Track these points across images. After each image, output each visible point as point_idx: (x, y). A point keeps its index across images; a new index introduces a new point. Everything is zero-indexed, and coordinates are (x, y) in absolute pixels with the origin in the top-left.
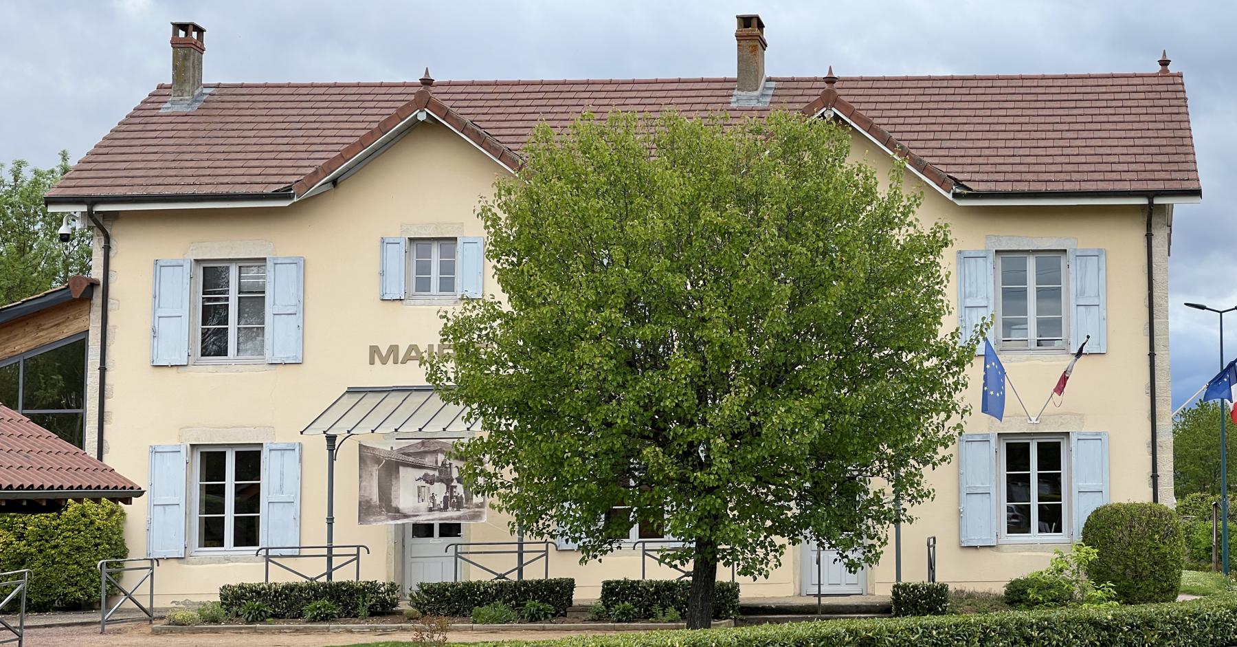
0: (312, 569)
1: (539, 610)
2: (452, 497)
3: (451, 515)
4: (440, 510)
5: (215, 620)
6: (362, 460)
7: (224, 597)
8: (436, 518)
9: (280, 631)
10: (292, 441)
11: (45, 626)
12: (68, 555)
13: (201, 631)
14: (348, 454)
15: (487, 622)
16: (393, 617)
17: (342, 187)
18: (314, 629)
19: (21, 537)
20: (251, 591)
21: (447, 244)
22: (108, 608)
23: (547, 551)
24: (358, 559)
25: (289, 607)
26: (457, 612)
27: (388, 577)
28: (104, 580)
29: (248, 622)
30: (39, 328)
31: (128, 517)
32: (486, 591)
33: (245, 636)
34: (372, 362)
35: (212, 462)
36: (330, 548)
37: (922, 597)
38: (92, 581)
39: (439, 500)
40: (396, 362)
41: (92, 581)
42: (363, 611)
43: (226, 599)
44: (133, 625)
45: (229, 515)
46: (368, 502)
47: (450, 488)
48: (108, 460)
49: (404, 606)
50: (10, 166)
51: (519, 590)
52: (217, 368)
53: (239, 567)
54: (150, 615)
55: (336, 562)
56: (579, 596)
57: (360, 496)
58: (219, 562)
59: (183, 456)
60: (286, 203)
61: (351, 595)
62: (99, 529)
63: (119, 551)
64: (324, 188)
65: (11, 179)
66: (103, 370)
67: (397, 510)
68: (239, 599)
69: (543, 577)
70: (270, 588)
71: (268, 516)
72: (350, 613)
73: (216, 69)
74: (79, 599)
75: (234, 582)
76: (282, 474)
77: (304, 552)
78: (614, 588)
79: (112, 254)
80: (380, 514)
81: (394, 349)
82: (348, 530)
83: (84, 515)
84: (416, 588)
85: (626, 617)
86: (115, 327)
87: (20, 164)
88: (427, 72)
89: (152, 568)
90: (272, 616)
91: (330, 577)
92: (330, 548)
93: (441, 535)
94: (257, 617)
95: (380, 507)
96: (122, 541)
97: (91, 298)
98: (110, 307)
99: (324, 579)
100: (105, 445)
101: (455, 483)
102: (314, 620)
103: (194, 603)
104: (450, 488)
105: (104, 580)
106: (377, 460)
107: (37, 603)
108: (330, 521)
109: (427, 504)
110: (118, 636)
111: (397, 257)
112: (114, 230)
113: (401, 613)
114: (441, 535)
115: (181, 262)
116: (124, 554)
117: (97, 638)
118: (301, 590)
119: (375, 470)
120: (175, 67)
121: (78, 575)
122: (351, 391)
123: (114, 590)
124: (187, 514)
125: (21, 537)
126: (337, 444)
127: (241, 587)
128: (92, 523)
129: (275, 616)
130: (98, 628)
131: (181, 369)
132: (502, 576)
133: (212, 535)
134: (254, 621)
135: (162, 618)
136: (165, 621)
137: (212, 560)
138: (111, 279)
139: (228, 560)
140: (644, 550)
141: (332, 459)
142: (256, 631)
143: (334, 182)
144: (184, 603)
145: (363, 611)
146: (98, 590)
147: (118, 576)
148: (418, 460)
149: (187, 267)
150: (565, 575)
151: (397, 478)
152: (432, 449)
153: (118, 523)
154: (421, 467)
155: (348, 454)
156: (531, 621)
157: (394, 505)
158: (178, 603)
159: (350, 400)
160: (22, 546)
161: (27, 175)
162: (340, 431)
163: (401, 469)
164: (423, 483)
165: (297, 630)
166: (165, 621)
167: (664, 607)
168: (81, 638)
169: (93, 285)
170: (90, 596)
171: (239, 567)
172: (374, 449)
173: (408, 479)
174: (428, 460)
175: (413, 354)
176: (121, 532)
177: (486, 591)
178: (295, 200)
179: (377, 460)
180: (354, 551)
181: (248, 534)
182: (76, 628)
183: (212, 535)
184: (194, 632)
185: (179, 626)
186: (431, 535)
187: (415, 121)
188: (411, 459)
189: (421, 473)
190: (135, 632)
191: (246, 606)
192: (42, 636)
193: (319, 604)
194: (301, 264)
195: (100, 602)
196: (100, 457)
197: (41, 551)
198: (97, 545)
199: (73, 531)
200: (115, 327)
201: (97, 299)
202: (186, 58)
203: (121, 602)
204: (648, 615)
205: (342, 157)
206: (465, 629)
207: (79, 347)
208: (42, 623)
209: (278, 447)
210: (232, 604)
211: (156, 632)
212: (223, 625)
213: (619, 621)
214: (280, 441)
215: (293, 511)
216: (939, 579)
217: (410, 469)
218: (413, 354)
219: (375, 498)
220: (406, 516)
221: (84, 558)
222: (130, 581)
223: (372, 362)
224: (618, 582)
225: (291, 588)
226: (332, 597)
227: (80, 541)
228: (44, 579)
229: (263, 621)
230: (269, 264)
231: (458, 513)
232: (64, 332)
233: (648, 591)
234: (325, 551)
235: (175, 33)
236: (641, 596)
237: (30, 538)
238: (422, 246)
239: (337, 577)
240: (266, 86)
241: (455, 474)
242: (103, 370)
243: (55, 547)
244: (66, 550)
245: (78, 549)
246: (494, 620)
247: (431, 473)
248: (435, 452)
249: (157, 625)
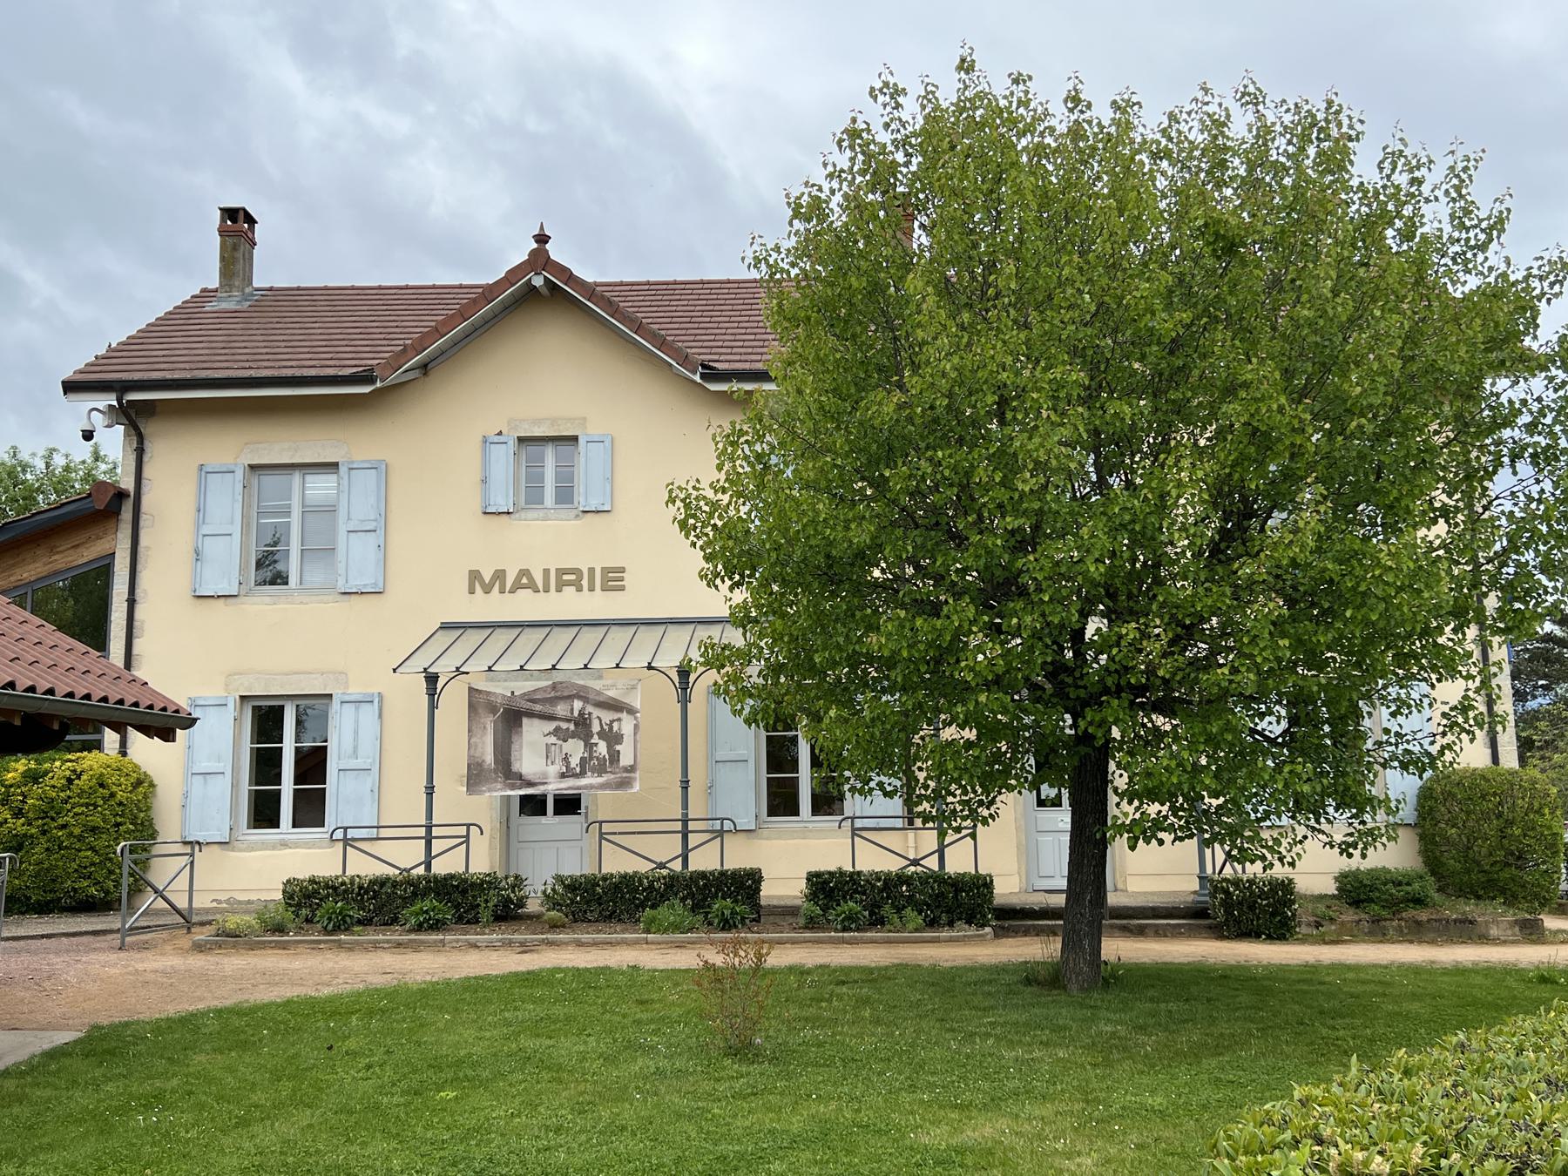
0: (404, 857)
2: (591, 758)
4: (576, 776)
5: (279, 929)
6: (472, 708)
7: (288, 896)
8: (554, 787)
9: (376, 946)
10: (370, 691)
11: (43, 937)
12: (80, 838)
13: (263, 945)
14: (454, 700)
15: (665, 931)
17: (435, 375)
18: (422, 942)
19: (18, 813)
20: (327, 887)
21: (565, 449)
22: (132, 909)
24: (467, 842)
25: (379, 910)
26: (610, 917)
27: (492, 867)
28: (126, 870)
29: (325, 931)
30: (52, 551)
31: (159, 790)
32: (651, 886)
33: (329, 955)
34: (472, 591)
35: (267, 720)
36: (429, 828)
37: (1263, 895)
38: (111, 872)
39: (575, 761)
40: (502, 592)
41: (111, 872)
42: (485, 916)
43: (291, 897)
44: (165, 935)
46: (480, 765)
47: (590, 747)
48: (140, 673)
49: (533, 906)
50: (42, 452)
54: (187, 920)
55: (437, 845)
56: (770, 892)
58: (274, 848)
59: (231, 711)
60: (366, 389)
61: (464, 892)
62: (121, 804)
63: (145, 830)
64: (411, 375)
65: (43, 466)
66: (132, 602)
67: (520, 777)
68: (309, 897)
69: (462, 870)
70: (352, 883)
71: (335, 784)
73: (268, 271)
74: (93, 896)
75: (303, 874)
76: (356, 732)
77: (384, 833)
78: (826, 882)
79: (146, 458)
81: (500, 575)
82: (454, 803)
83: (102, 785)
84: (550, 881)
85: (850, 923)
86: (148, 548)
87: (52, 451)
88: (542, 228)
89: (192, 855)
90: (360, 922)
92: (429, 828)
93: (556, 813)
94: (341, 924)
95: (495, 771)
96: (151, 820)
97: (118, 513)
98: (142, 523)
99: (421, 870)
100: (136, 624)
101: (595, 739)
102: (419, 928)
103: (240, 902)
104: (590, 747)
105: (126, 870)
106: (493, 709)
107: (38, 901)
108: (430, 791)
109: (558, 767)
110: (148, 954)
111: (503, 458)
112: (148, 428)
114: (556, 813)
115: (232, 468)
116: (153, 835)
117: (113, 957)
118: (395, 884)
119: (489, 723)
120: (222, 259)
121: (93, 864)
122: (445, 627)
123: (139, 885)
125: (18, 813)
126: (439, 686)
127: (312, 881)
128: (113, 795)
130: (115, 939)
131: (230, 600)
132: (662, 866)
133: (264, 813)
134: (337, 929)
135: (202, 924)
137: (264, 846)
138: (145, 489)
139: (285, 845)
140: (601, 834)
141: (433, 707)
142: (340, 945)
143: (424, 368)
144: (227, 901)
145: (485, 916)
146: (118, 884)
147: (144, 864)
148: (548, 709)
149: (239, 474)
150: (747, 864)
153: (146, 797)
155: (454, 700)
156: (723, 929)
157: (515, 767)
158: (219, 902)
159: (447, 637)
160: (19, 825)
161: (59, 461)
162: (444, 668)
163: (525, 721)
164: (553, 739)
165: (399, 945)
166: (211, 929)
167: (899, 910)
168: (93, 956)
169: (121, 495)
170: (107, 892)
172: (489, 693)
173: (534, 733)
174: (561, 709)
175: (524, 580)
176: (149, 808)
177: (651, 886)
178: (379, 384)
180: (462, 831)
181: (311, 810)
182: (85, 939)
183: (264, 813)
184: (253, 947)
187: (531, 289)
188: (538, 707)
189: (552, 726)
190: (168, 948)
191: (321, 909)
192: (36, 953)
193: (426, 905)
194: (381, 469)
195: (120, 900)
196: (128, 664)
197: (44, 833)
198: (118, 825)
199: (87, 805)
200: (148, 548)
201: (127, 514)
202: (235, 248)
203: (148, 900)
204: (878, 922)
205: (437, 332)
206: (636, 942)
207: (104, 570)
208: (40, 932)
210: (299, 906)
211: (199, 948)
212: (291, 937)
213: (844, 930)
214: (355, 691)
215: (369, 781)
216: (858, 868)
217: (536, 721)
218: (524, 580)
220: (531, 784)
221: (100, 843)
222: (165, 870)
223: (472, 591)
224: (830, 873)
225: (382, 882)
226: (438, 894)
227: (96, 820)
228: (48, 870)
229: (347, 930)
230: (343, 469)
231: (600, 780)
232: (88, 554)
233: (874, 886)
235: (223, 220)
236: (864, 893)
237: (31, 815)
238: (533, 449)
239: (440, 867)
240: (326, 288)
241: (596, 728)
242: (132, 602)
243: (64, 827)
244: (77, 831)
245: (94, 830)
246: (676, 927)
247: (564, 725)
248: (571, 698)
249: (201, 935)
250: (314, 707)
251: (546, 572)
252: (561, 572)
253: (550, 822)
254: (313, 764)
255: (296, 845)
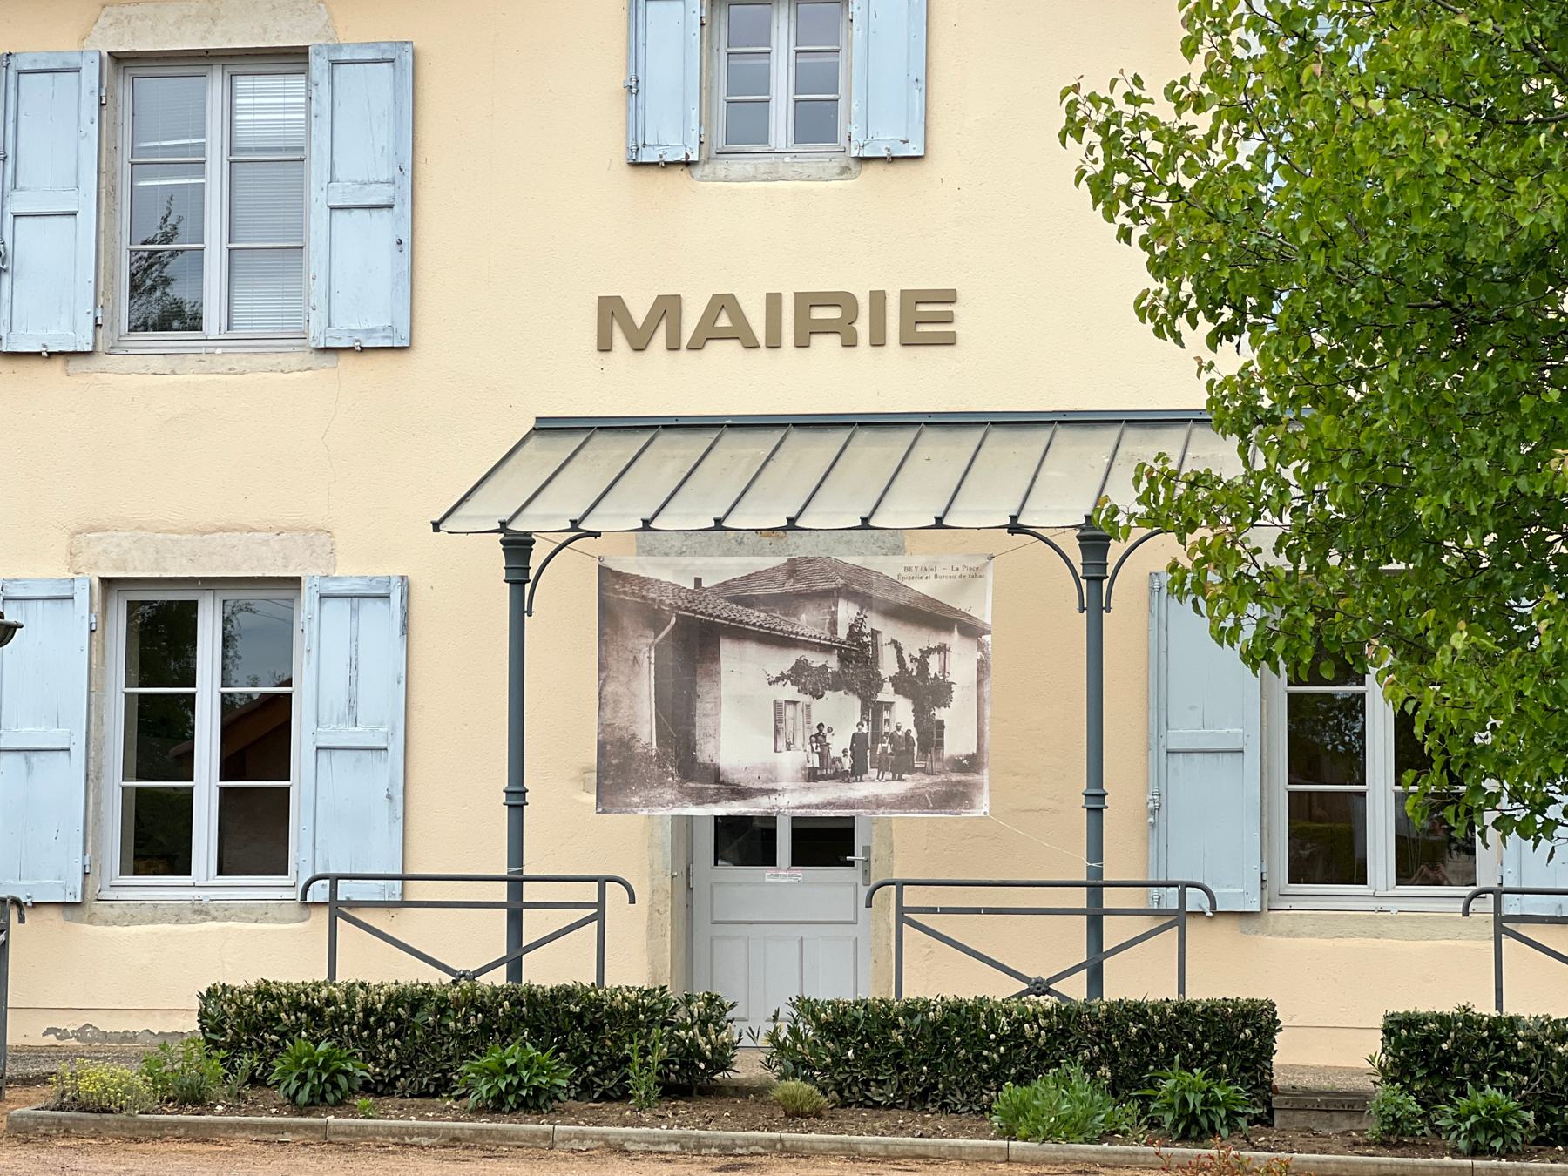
0: (459, 946)
1: (1209, 1102)
2: (877, 736)
3: (820, 801)
5: (194, 1098)
6: (608, 614)
8: (791, 800)
10: (381, 572)
13: (158, 1133)
14: (566, 592)
16: (708, 1109)
18: (504, 1136)
20: (296, 1007)
23: (601, 905)
24: (600, 917)
25: (408, 1063)
27: (654, 976)
34: (605, 346)
35: (159, 632)
36: (516, 882)
39: (839, 744)
40: (673, 346)
42: (642, 1083)
43: (218, 1028)
45: (206, 784)
47: (874, 711)
49: (748, 1067)
51: (1123, 1035)
52: (176, 360)
53: (222, 939)
55: (535, 925)
56: (1292, 1057)
57: (603, 726)
59: (81, 613)
61: (595, 1029)
67: (715, 774)
68: (257, 1029)
70: (350, 1000)
71: (308, 779)
72: (603, 1085)
75: (243, 976)
76: (353, 665)
77: (418, 891)
78: (1430, 1040)
80: (662, 784)
81: (667, 308)
84: (787, 1012)
90: (367, 1088)
91: (515, 971)
92: (516, 882)
94: (326, 1092)
95: (661, 760)
99: (499, 977)
101: (886, 694)
102: (496, 1106)
104: (874, 711)
106: (652, 617)
108: (516, 800)
113: (741, 1091)
114: (799, 859)
115: (74, 61)
118: (443, 1007)
119: (645, 649)
122: (547, 428)
124: (92, 777)
126: (535, 563)
127: (264, 992)
129: (378, 1088)
131: (76, 364)
132: (1041, 987)
133: (157, 841)
134: (317, 1102)
136: (49, 1093)
137: (157, 914)
139: (202, 912)
140: (901, 911)
141: (520, 611)
142: (325, 1137)
144: (80, 1034)
145: (642, 1083)
148: (777, 621)
149: (90, 75)
151: (714, 676)
152: (819, 586)
154: (785, 641)
155: (566, 592)
156: (1184, 1138)
157: (705, 753)
158: (62, 1034)
163: (727, 647)
164: (789, 691)
165: (454, 1141)
166: (49, 1093)
171: (222, 939)
172: (643, 582)
173: (745, 679)
174: (808, 622)
175: (724, 321)
179: (652, 617)
180: (589, 892)
181: (256, 836)
183: (157, 841)
185: (88, 1114)
186: (767, 857)
188: (756, 617)
189: (785, 660)
191: (269, 1048)
193: (513, 1054)
209: (343, 588)
210: (235, 1046)
212: (218, 1116)
213: (1475, 1152)
214: (351, 571)
215: (385, 773)
216: (1509, 1010)
217: (751, 649)
218: (724, 321)
219: (646, 731)
223: (605, 346)
225: (415, 1000)
226: (537, 1032)
230: (318, 64)
234: (500, 892)
239: (542, 972)
241: (888, 666)
247: (815, 660)
250: (266, 602)
251: (774, 301)
252: (807, 302)
253: (784, 876)
254: (260, 734)
255: (227, 913)
